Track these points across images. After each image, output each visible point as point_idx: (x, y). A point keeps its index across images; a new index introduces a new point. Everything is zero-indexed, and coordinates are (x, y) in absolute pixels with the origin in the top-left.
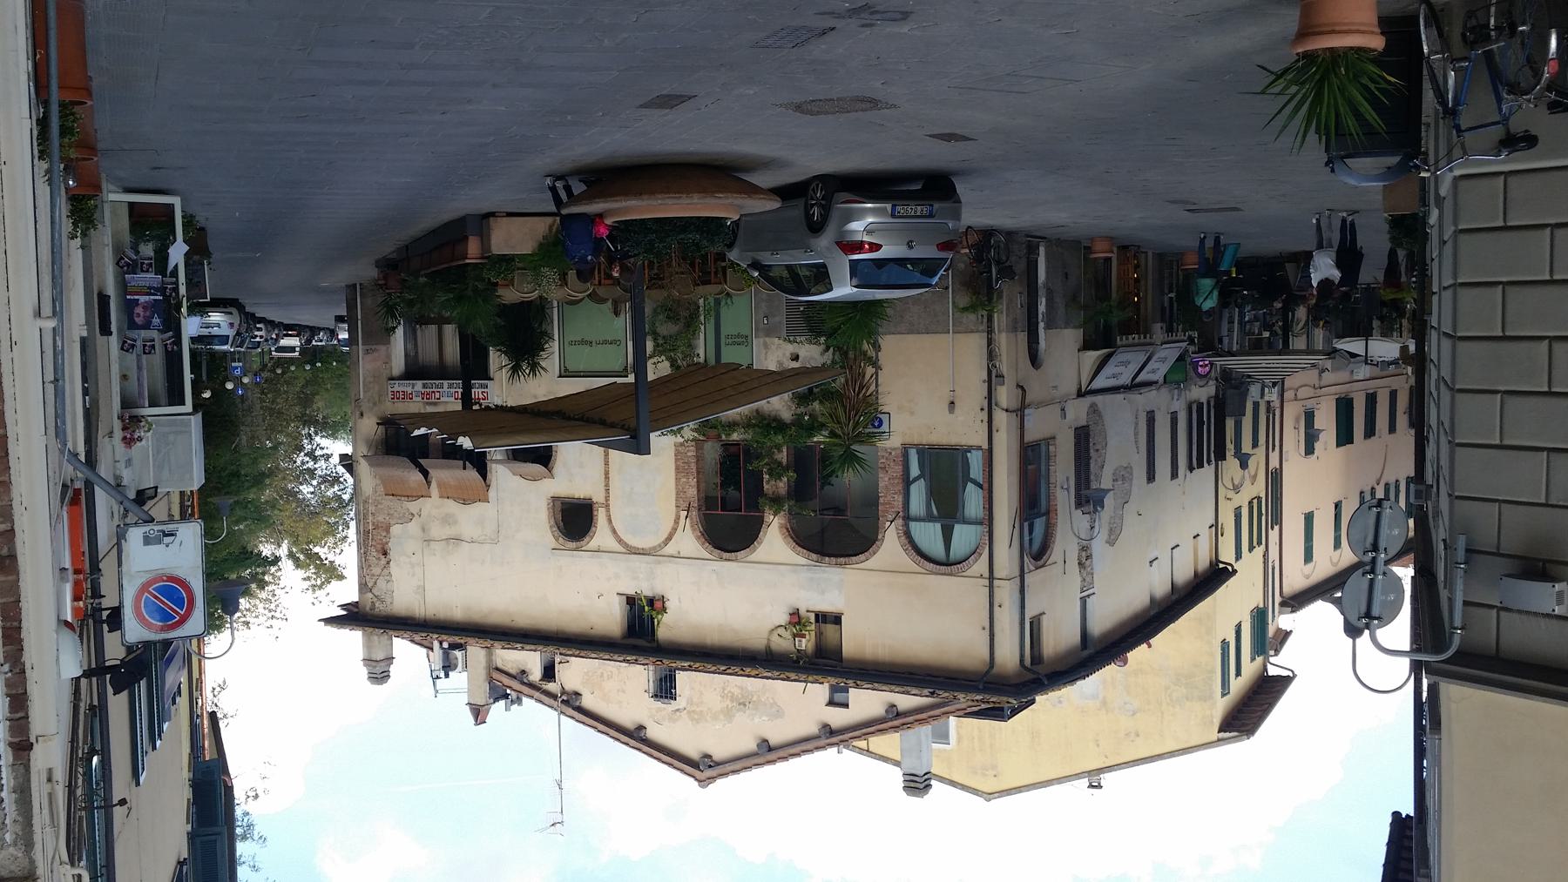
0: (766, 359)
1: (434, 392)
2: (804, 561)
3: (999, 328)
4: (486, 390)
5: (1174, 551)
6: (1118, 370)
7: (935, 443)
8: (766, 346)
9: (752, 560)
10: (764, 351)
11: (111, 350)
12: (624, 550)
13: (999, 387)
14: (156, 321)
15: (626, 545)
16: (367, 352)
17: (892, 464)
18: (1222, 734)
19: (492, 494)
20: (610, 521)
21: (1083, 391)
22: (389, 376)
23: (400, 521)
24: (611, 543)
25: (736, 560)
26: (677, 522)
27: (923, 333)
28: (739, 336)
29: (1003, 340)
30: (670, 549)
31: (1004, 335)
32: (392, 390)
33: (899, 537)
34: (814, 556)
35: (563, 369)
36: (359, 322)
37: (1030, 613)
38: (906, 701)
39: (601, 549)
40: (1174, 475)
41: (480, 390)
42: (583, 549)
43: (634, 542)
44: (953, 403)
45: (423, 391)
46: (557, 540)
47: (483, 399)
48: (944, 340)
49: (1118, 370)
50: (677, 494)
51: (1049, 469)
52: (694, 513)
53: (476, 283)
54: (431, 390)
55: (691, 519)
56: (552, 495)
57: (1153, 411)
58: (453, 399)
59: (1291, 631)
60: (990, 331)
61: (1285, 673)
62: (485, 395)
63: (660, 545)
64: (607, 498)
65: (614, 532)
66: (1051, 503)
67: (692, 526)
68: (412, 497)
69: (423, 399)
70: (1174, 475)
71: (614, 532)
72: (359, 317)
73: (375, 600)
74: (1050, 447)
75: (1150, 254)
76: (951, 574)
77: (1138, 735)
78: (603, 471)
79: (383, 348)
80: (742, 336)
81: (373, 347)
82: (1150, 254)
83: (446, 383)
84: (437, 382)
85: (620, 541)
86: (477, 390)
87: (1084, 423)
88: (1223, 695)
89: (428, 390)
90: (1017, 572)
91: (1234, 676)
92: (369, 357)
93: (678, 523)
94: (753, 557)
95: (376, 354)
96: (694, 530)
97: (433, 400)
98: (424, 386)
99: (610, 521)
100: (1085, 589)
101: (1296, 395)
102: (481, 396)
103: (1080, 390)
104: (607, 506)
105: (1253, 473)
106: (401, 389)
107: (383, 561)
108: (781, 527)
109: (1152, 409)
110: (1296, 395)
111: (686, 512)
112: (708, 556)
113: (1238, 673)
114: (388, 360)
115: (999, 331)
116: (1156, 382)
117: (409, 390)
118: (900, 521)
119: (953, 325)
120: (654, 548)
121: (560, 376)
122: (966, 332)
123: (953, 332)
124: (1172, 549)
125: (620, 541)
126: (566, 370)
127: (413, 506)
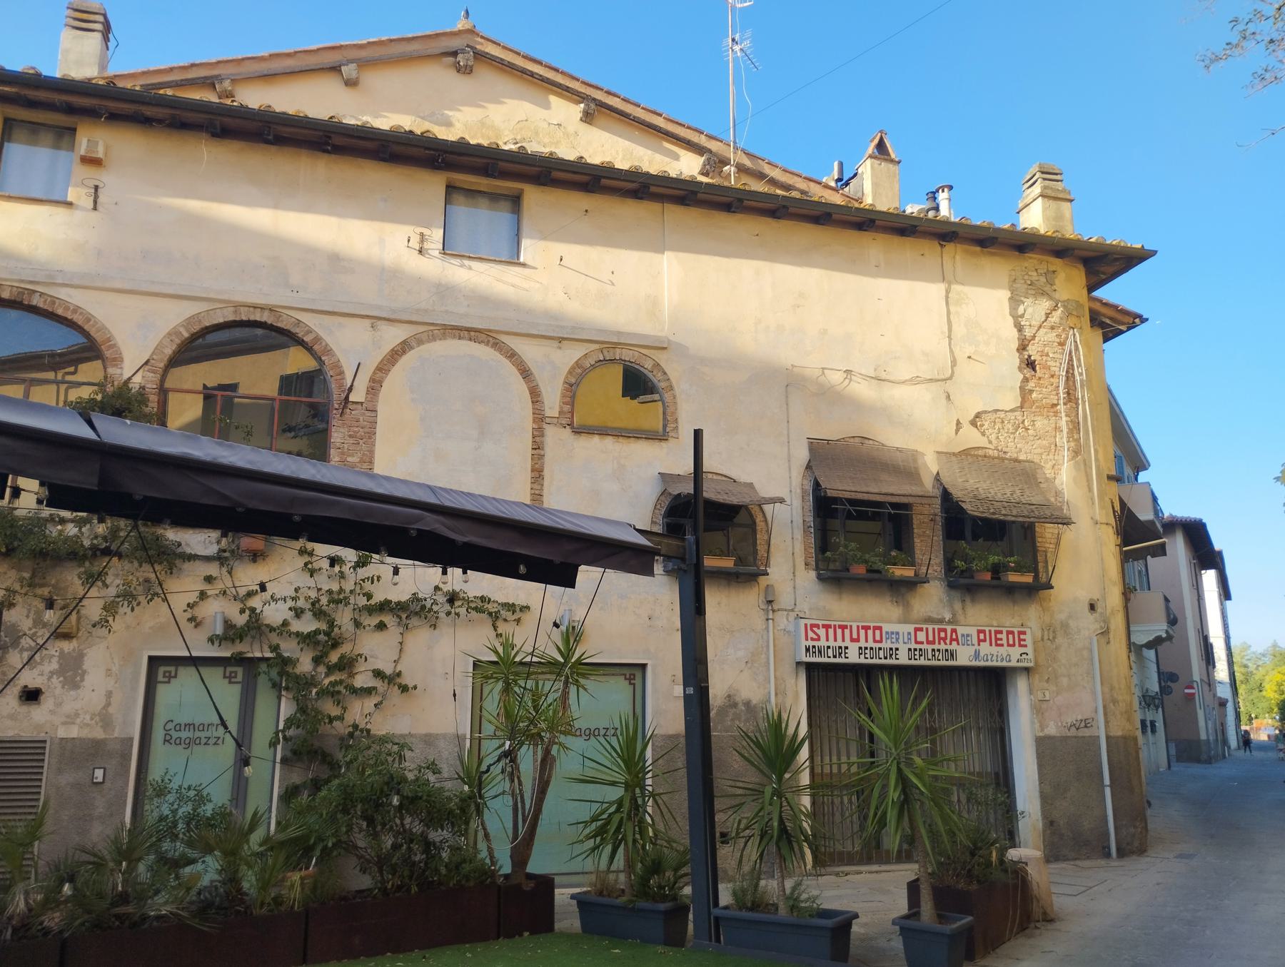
0: (109, 694)
1: (928, 642)
2: (62, 294)
4: (811, 643)
8: (105, 720)
9: (185, 303)
10: (111, 710)
12: (504, 338)
14: (438, 844)
15: (497, 345)
16: (1087, 724)
19: (802, 455)
20: (535, 394)
22: (1036, 679)
23: (1002, 415)
24: (530, 352)
25: (237, 306)
26: (375, 386)
28: (189, 743)
30: (393, 336)
32: (1023, 650)
35: (638, 681)
36: (1107, 781)
38: (253, 98)
39: (367, 322)
41: (823, 643)
42: (597, 346)
43: (483, 352)
45: (954, 646)
46: (657, 365)
47: (817, 626)
50: (371, 434)
52: (337, 397)
53: (94, 916)
54: (936, 647)
55: (341, 386)
56: (663, 444)
58: (887, 627)
59: (1147, 320)
62: (811, 634)
63: (420, 342)
64: (538, 435)
65: (526, 373)
67: (342, 373)
68: (977, 456)
69: (954, 631)
71: (526, 373)
72: (1108, 791)
73: (1047, 289)
78: (546, 483)
79: (1052, 730)
80: (179, 742)
81: (1073, 732)
83: (903, 659)
84: (922, 662)
85: (512, 355)
86: (831, 643)
89: (943, 647)
92: (1087, 714)
93: (372, 380)
94: (191, 309)
95: (1070, 719)
97: (930, 627)
98: (952, 655)
99: (535, 394)
102: (822, 632)
104: (540, 418)
106: (1003, 651)
107: (1033, 351)
111: (352, 398)
112: (305, 318)
114: (1038, 709)
117: (985, 648)
120: (433, 338)
121: (643, 666)
125: (512, 355)
126: (631, 680)
127: (972, 438)
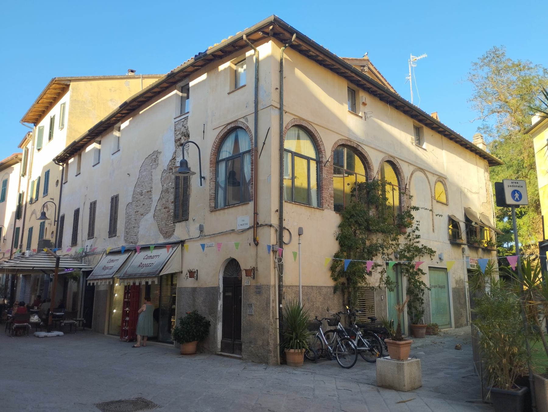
2: (364, 147)
3: (275, 287)
5: (98, 162)
6: (112, 264)
7: (308, 208)
11: (404, 296)
13: (275, 243)
15: (425, 174)
17: (328, 198)
18: (68, 84)
21: (181, 245)
27: (314, 286)
29: (273, 280)
31: (272, 283)
33: (324, 150)
34: (360, 149)
37: (61, 214)
40: (93, 206)
44: (299, 235)
48: (304, 282)
49: (112, 264)
51: (215, 191)
57: (109, 238)
60: (280, 287)
61: (25, 123)
66: (214, 169)
70: (93, 206)
74: (214, 205)
75: (106, 333)
76: (304, 120)
77: (110, 90)
82: (106, 333)
85: (427, 177)
87: (178, 225)
88: (64, 104)
90: (260, 113)
91: (66, 103)
96: (404, 177)
100: (183, 120)
101: (4, 255)
103: (183, 246)
105: (34, 215)
108: (373, 170)
109: (111, 239)
110: (4, 255)
112: (399, 161)
113: (52, 120)
115: (275, 286)
116: (107, 255)
118: (324, 160)
119: (299, 291)
122: (292, 286)
123: (299, 286)
124: (99, 163)
125: (427, 177)
